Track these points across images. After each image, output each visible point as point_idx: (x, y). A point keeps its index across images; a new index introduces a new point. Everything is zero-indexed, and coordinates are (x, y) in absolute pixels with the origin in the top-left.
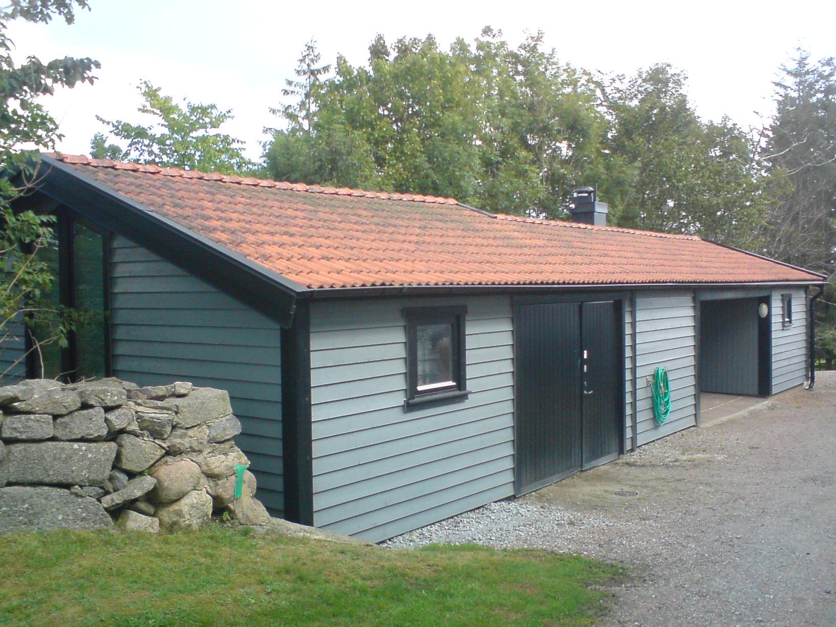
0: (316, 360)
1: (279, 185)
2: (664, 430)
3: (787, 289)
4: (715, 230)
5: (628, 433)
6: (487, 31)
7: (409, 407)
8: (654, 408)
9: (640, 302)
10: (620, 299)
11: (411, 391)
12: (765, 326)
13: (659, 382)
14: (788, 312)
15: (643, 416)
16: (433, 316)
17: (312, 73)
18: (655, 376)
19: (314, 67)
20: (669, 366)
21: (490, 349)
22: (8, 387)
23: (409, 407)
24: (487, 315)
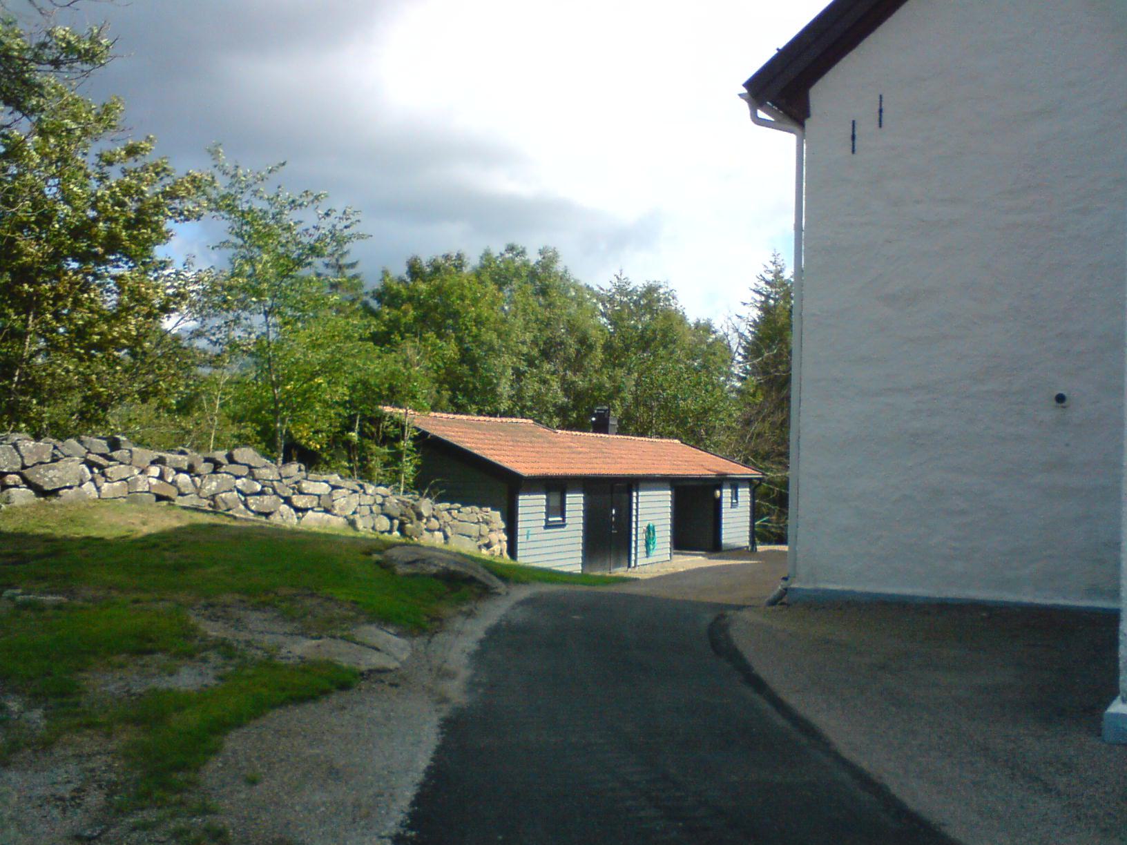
0: (520, 503)
1: (458, 417)
2: (650, 560)
3: (735, 483)
4: (695, 438)
5: (633, 557)
6: (511, 248)
7: (547, 527)
8: (647, 545)
9: (641, 485)
10: (632, 484)
11: (547, 520)
12: (718, 502)
13: (650, 530)
14: (735, 496)
15: (642, 549)
16: (555, 486)
17: (340, 267)
18: (648, 527)
19: (342, 262)
20: (656, 523)
21: (575, 502)
22: (176, 524)
23: (547, 527)
24: (574, 491)
